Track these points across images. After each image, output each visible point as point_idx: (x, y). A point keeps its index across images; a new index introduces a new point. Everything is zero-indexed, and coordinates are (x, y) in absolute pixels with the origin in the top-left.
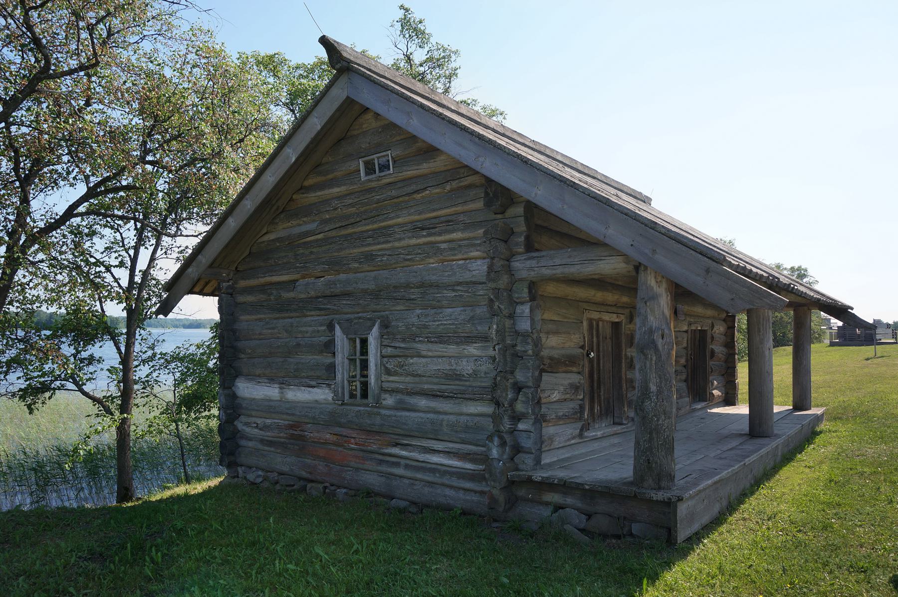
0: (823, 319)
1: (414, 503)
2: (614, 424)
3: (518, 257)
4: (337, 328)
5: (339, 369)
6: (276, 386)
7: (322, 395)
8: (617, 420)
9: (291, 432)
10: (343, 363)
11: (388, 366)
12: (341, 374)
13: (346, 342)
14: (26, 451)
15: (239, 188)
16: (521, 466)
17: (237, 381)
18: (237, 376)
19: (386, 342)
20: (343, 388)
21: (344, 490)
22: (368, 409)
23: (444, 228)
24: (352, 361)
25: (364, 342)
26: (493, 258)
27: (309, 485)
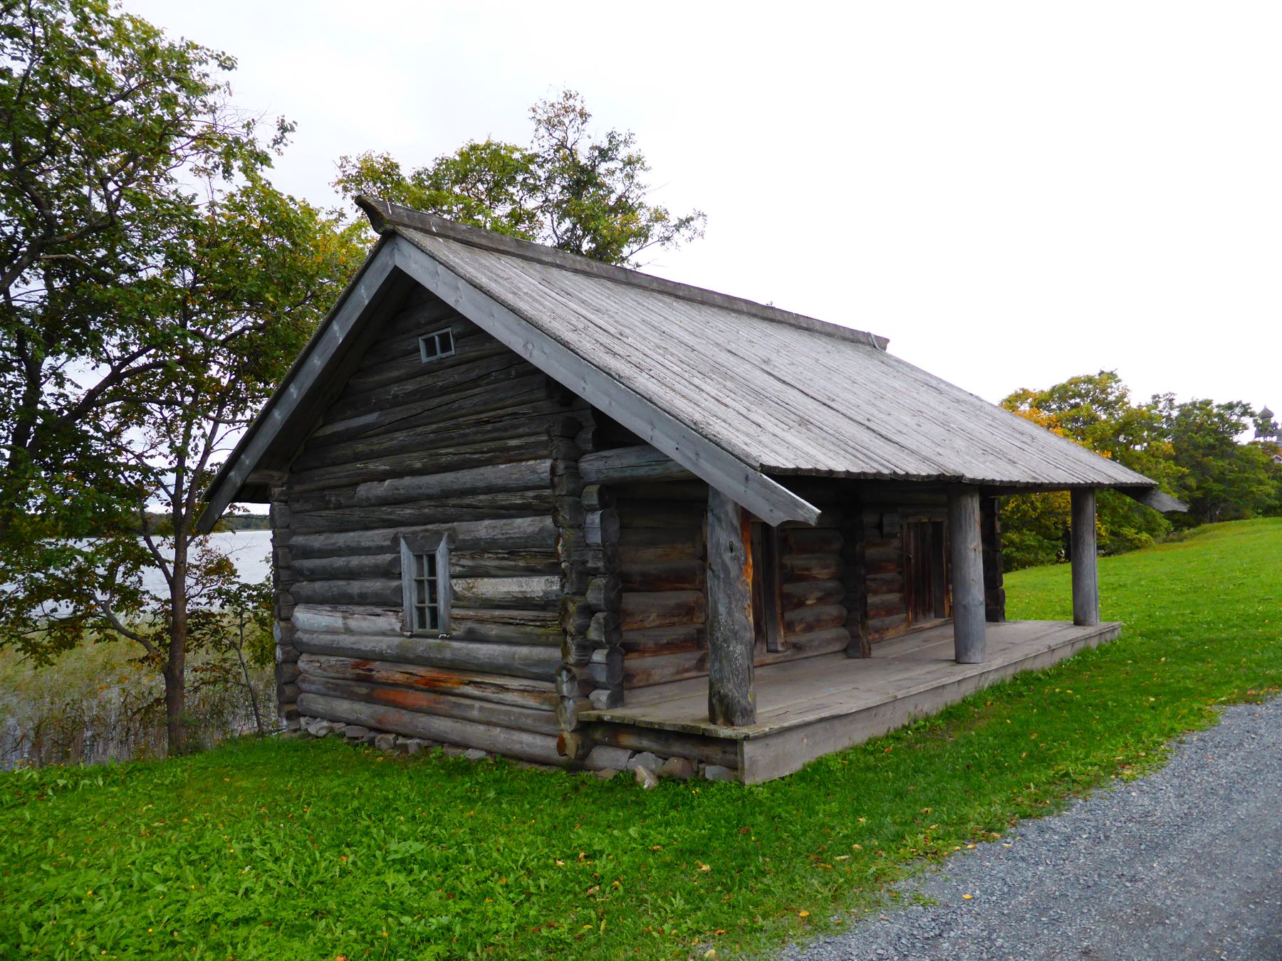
0: (301, 653)
1: (490, 752)
2: (768, 651)
3: (588, 457)
4: (403, 542)
5: (406, 595)
6: (339, 614)
7: (388, 621)
8: (772, 647)
9: (358, 671)
10: (410, 586)
11: (456, 588)
12: (410, 598)
13: (413, 559)
14: (1261, 595)
15: (307, 344)
16: (596, 705)
17: (296, 609)
18: (296, 604)
19: (453, 561)
20: (411, 614)
21: (417, 741)
22: (438, 641)
23: (509, 422)
24: (420, 583)
25: (432, 559)
26: (556, 460)
27: (379, 737)
